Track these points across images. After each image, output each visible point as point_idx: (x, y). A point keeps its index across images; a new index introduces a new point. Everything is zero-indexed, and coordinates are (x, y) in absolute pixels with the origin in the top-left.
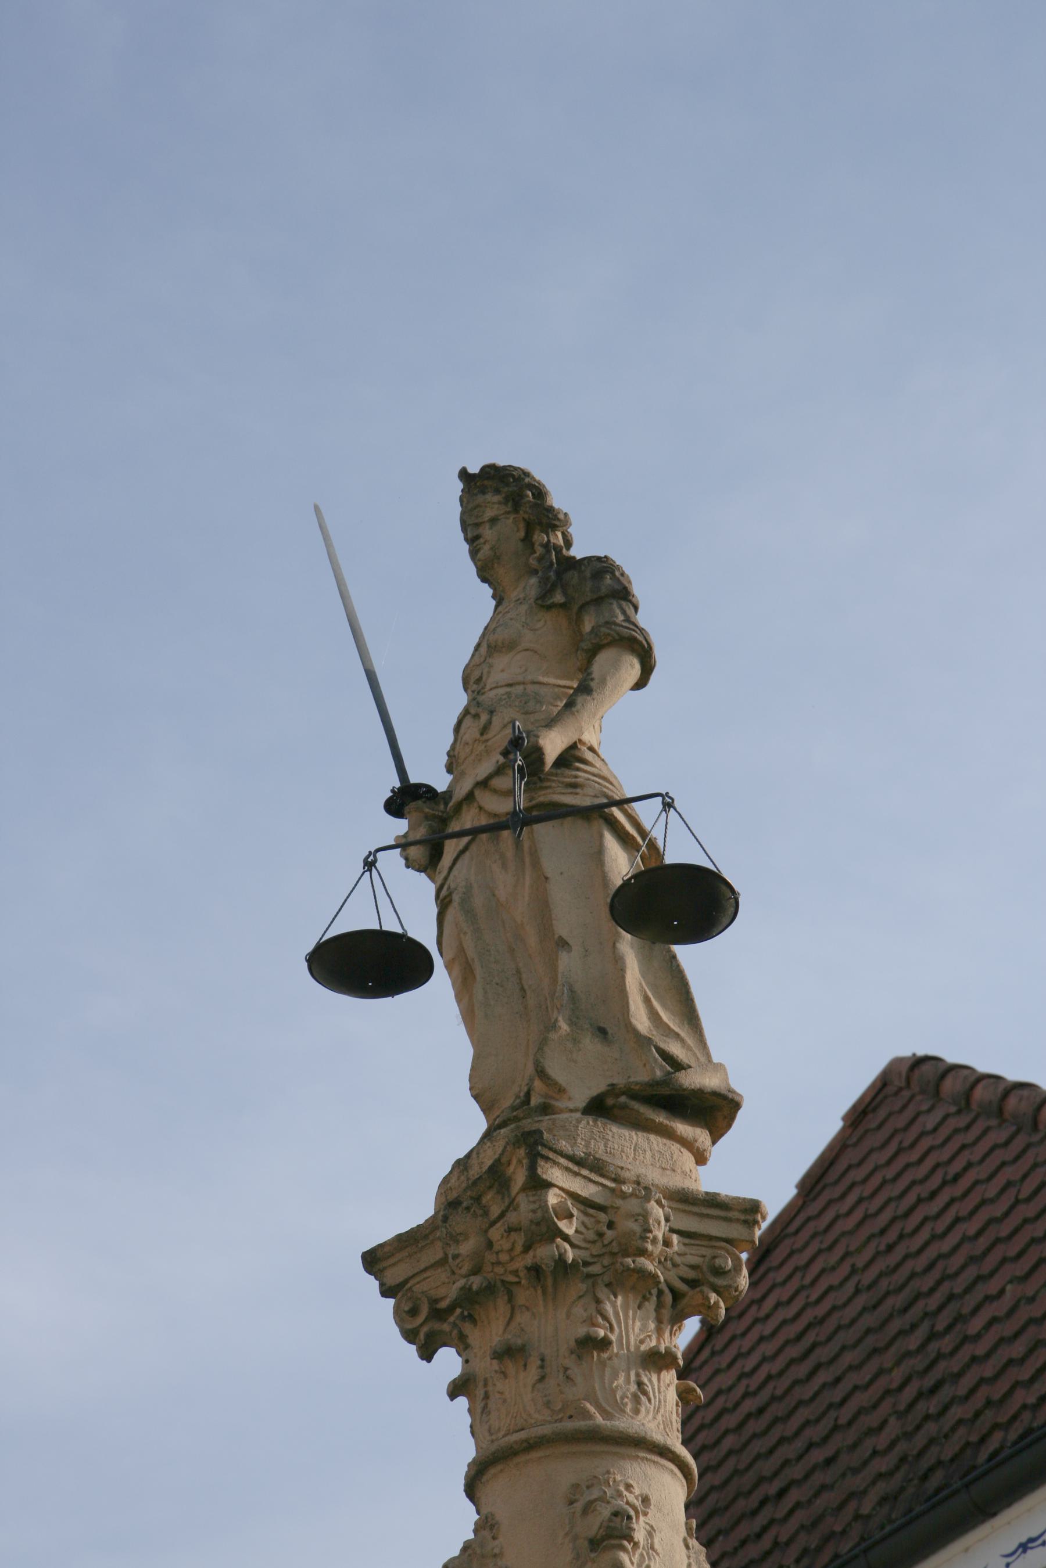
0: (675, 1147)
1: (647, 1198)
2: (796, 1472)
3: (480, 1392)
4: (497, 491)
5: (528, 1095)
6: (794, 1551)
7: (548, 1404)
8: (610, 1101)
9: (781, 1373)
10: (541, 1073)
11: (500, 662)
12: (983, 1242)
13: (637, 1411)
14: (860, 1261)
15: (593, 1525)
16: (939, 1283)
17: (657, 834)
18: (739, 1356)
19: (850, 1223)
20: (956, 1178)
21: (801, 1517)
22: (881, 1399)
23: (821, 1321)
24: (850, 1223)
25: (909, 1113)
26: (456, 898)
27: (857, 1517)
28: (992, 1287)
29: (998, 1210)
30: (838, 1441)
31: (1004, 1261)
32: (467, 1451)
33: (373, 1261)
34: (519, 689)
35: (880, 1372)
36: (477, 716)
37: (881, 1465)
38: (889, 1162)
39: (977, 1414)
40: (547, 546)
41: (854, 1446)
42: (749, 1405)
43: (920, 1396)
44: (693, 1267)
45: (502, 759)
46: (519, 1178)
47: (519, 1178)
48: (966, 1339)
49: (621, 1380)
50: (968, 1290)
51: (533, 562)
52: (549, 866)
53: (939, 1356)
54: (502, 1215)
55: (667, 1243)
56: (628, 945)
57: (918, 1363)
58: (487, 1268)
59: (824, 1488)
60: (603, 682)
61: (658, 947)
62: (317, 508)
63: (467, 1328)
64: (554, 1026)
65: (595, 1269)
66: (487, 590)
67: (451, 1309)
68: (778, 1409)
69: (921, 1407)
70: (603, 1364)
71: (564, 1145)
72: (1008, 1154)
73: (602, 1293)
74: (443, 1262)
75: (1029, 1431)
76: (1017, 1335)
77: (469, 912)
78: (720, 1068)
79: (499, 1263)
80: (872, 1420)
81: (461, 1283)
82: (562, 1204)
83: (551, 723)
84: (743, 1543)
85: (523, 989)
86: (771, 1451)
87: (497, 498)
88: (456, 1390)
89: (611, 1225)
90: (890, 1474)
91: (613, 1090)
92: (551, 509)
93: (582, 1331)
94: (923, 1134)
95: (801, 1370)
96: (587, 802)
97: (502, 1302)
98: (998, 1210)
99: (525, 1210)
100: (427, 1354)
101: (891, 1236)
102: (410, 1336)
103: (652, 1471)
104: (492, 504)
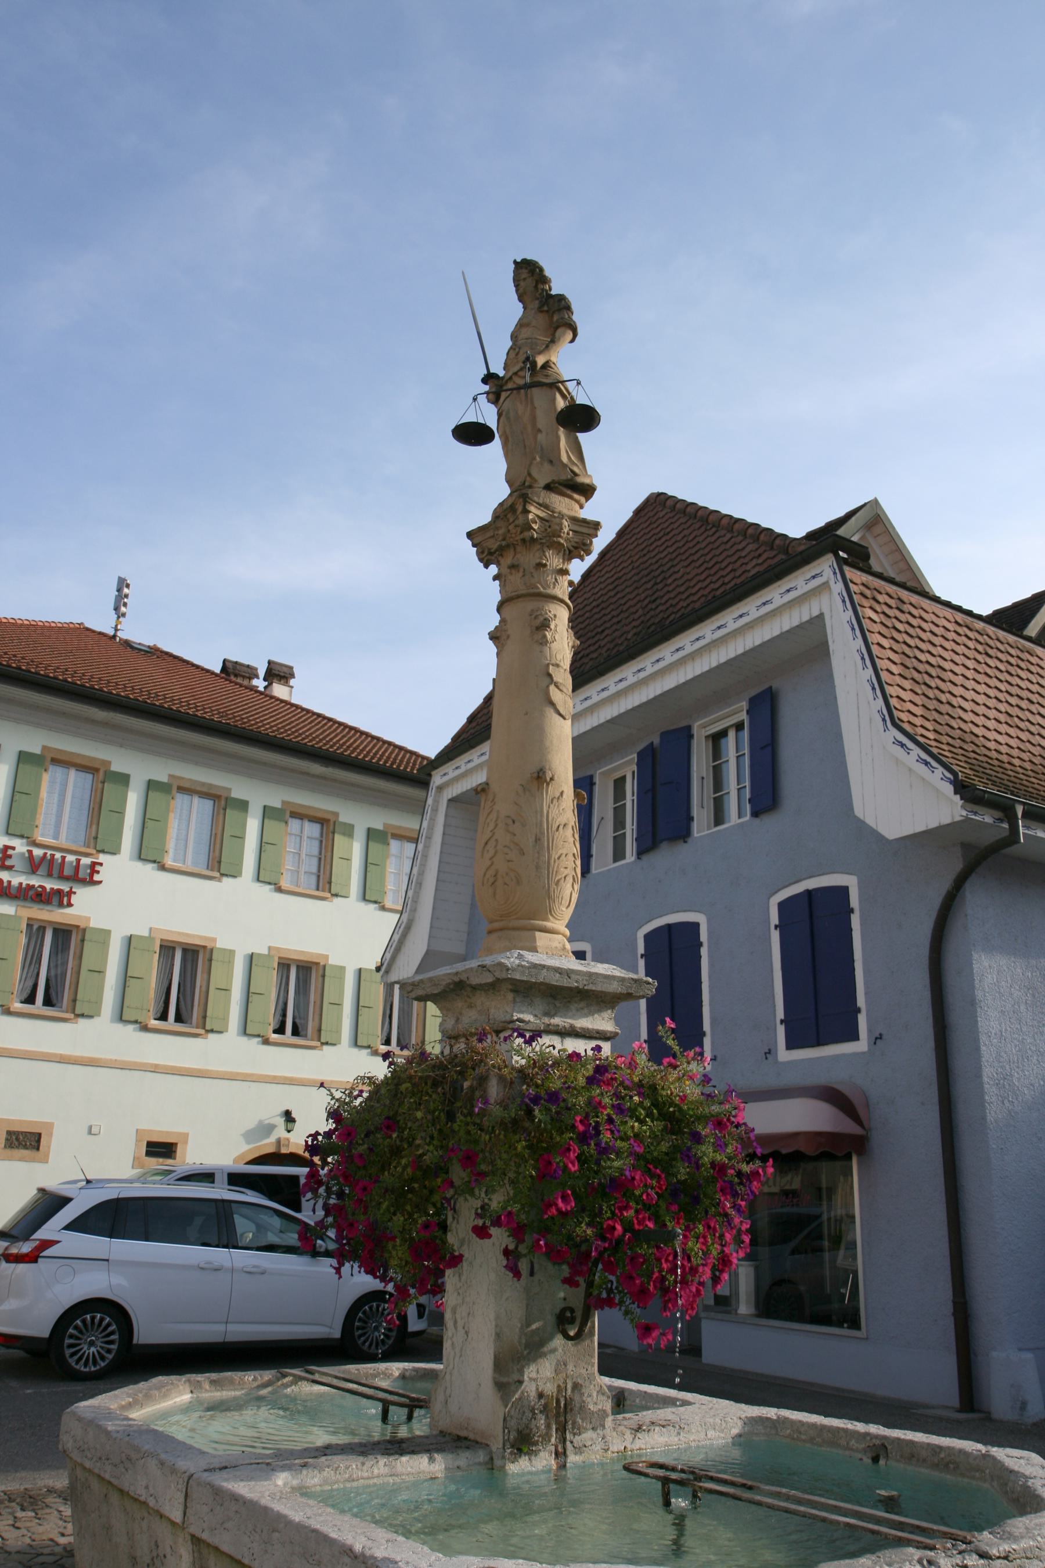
0: (573, 502)
1: (562, 518)
2: (608, 625)
3: (503, 580)
4: (526, 268)
5: (525, 482)
6: (605, 649)
7: (525, 584)
8: (552, 485)
9: (606, 594)
10: (530, 475)
11: (524, 330)
12: (674, 555)
13: (554, 588)
14: (635, 559)
15: (537, 623)
16: (659, 567)
17: (574, 394)
18: (593, 588)
19: (632, 547)
20: (668, 533)
21: (609, 639)
22: (637, 603)
23: (620, 578)
24: (632, 547)
25: (655, 511)
26: (504, 413)
27: (626, 639)
28: (676, 570)
29: (681, 544)
30: (623, 616)
31: (681, 560)
32: (498, 598)
33: (470, 535)
34: (530, 341)
35: (638, 595)
36: (515, 349)
37: (635, 623)
38: (647, 528)
39: (667, 609)
40: (543, 290)
41: (627, 618)
42: (595, 604)
43: (650, 602)
44: (576, 542)
45: (522, 365)
46: (520, 509)
47: (520, 509)
48: (666, 585)
49: (550, 577)
50: (669, 569)
51: (537, 295)
52: (537, 403)
53: (657, 590)
54: (514, 521)
55: (568, 534)
56: (561, 432)
57: (650, 592)
58: (507, 538)
59: (616, 630)
60: (559, 339)
61: (572, 433)
62: (463, 273)
63: (500, 558)
64: (534, 459)
65: (544, 541)
66: (521, 305)
67: (495, 552)
68: (604, 605)
69: (650, 606)
70: (544, 572)
71: (536, 499)
72: (685, 526)
73: (545, 549)
74: (493, 537)
75: (683, 614)
76: (682, 584)
77: (508, 418)
78: (590, 476)
79: (511, 537)
81: (498, 543)
82: (534, 519)
83: (540, 353)
84: (589, 646)
85: (525, 446)
86: (601, 618)
87: (527, 271)
88: (495, 578)
89: (550, 527)
90: (638, 626)
91: (553, 482)
92: (545, 276)
93: (538, 561)
94: (659, 518)
95: (612, 593)
96: (551, 381)
97: (512, 550)
98: (681, 544)
99: (521, 520)
100: (486, 566)
101: (645, 552)
102: (481, 560)
103: (557, 607)
104: (524, 274)
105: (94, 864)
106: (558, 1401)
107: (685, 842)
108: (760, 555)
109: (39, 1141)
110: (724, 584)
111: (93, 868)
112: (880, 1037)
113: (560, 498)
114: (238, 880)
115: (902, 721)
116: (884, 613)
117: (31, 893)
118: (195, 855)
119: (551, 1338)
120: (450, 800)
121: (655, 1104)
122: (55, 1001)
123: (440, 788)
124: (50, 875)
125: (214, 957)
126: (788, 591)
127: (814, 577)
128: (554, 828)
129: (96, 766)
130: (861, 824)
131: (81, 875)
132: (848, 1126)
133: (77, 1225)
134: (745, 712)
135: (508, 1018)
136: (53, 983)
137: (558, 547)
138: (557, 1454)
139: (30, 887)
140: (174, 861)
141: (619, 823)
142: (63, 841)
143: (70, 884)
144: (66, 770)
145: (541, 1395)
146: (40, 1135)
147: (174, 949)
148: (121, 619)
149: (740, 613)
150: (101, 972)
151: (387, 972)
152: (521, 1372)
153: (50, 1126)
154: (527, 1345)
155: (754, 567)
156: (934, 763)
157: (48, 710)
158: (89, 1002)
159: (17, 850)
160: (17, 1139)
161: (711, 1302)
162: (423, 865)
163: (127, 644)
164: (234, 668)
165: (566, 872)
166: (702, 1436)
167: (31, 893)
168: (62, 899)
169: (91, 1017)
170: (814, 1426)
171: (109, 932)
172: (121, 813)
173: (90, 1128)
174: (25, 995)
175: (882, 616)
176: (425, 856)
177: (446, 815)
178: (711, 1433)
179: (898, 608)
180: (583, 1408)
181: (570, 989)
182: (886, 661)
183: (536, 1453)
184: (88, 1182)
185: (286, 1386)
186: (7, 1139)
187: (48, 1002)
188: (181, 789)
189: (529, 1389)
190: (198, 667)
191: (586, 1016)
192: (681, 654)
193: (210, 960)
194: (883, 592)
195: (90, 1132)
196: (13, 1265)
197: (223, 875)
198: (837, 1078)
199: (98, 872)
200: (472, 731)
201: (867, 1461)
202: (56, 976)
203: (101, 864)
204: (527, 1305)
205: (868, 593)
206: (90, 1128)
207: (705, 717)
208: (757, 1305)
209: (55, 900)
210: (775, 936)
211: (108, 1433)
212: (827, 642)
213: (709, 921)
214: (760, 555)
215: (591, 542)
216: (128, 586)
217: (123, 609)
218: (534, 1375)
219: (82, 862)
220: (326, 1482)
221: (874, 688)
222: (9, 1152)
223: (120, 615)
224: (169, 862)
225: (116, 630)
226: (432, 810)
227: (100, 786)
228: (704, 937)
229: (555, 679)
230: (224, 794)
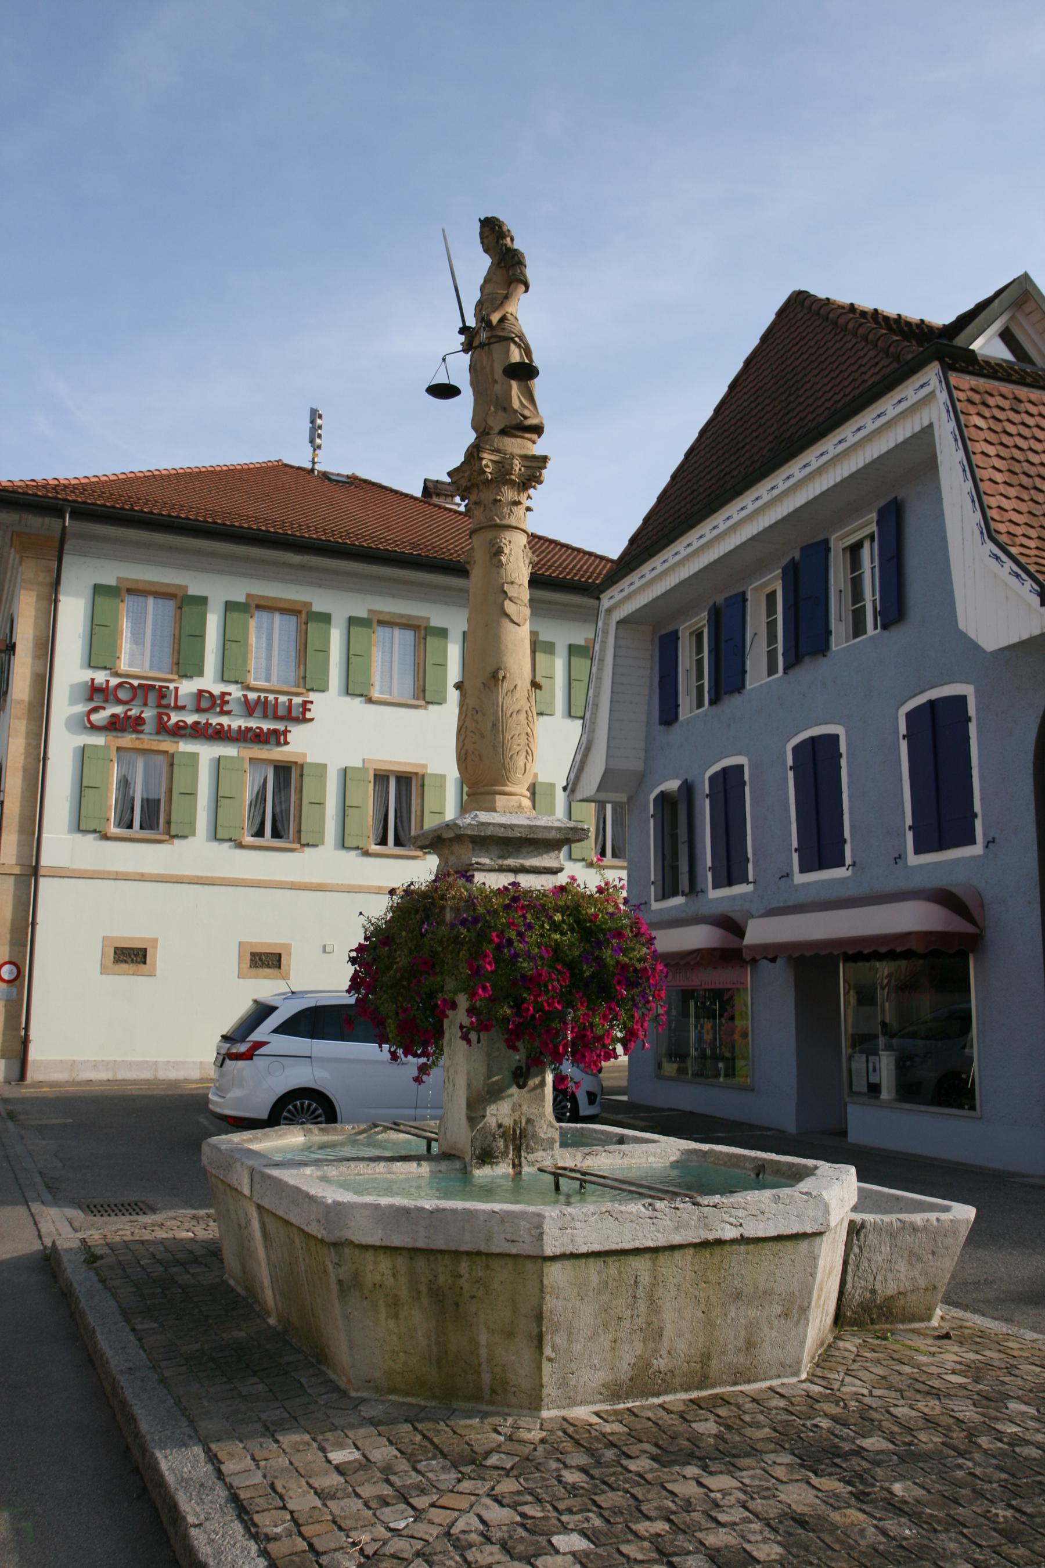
15: (494, 549)
19: (772, 353)
71: (488, 447)
80: (770, 423)
91: (506, 427)
95: (753, 405)
99: (476, 467)
105: (305, 703)
106: (514, 1131)
107: (825, 656)
108: (877, 363)
109: (279, 960)
110: (844, 396)
111: (305, 706)
112: (993, 841)
113: (513, 440)
114: (444, 706)
115: (1000, 533)
116: (994, 418)
117: (250, 735)
118: (402, 685)
119: (509, 1087)
120: (618, 622)
121: (578, 921)
122: (282, 833)
123: (609, 611)
124: (265, 716)
125: (426, 782)
126: (900, 402)
127: (922, 386)
128: (508, 715)
129: (299, 608)
130: (964, 636)
131: (294, 714)
132: (959, 925)
133: (285, 1028)
134: (875, 524)
135: (468, 862)
136: (279, 818)
137: (512, 483)
138: (514, 1166)
139: (249, 729)
140: (381, 693)
141: (772, 638)
142: (275, 684)
143: (285, 723)
144: (270, 615)
145: (500, 1126)
146: (280, 955)
147: (388, 777)
148: (317, 452)
149: (839, 439)
150: (321, 804)
151: (573, 791)
152: (485, 1110)
153: (288, 946)
154: (489, 1092)
155: (871, 376)
156: (1024, 576)
157: (247, 559)
158: (313, 832)
159: (233, 696)
160: (260, 959)
161: (865, 1090)
162: (598, 687)
163: (325, 476)
164: (436, 488)
165: (518, 748)
166: (644, 1160)
167: (250, 735)
168: (277, 738)
169: (315, 846)
170: (727, 1154)
171: (325, 766)
172: (326, 651)
173: (324, 947)
174: (255, 829)
175: (991, 421)
176: (599, 679)
177: (616, 637)
178: (651, 1159)
179: (1012, 409)
180: (534, 1136)
181: (520, 838)
182: (990, 470)
183: (497, 1163)
184: (293, 993)
185: (378, 1133)
186: (251, 960)
187: (276, 834)
188: (381, 623)
189: (491, 1121)
190: (396, 492)
191: (536, 856)
192: (808, 470)
193: (423, 786)
194: (995, 393)
195: (324, 951)
196: (234, 1062)
197: (428, 703)
198: (954, 881)
199: (309, 710)
200: (633, 553)
201: (753, 1176)
202: (281, 811)
203: (312, 702)
204: (488, 1065)
205: (976, 398)
206: (324, 947)
207: (841, 529)
208: (898, 1092)
209: (273, 740)
210: (904, 745)
211: (220, 1150)
212: (936, 454)
213: (847, 732)
214: (877, 363)
215: (541, 474)
216: (320, 417)
217: (318, 441)
218: (494, 1112)
219: (293, 702)
220: (341, 1174)
221: (973, 501)
222: (254, 971)
223: (317, 448)
224: (376, 694)
225: (314, 463)
226: (603, 632)
227: (304, 627)
228: (843, 748)
229: (509, 595)
230: (424, 624)
